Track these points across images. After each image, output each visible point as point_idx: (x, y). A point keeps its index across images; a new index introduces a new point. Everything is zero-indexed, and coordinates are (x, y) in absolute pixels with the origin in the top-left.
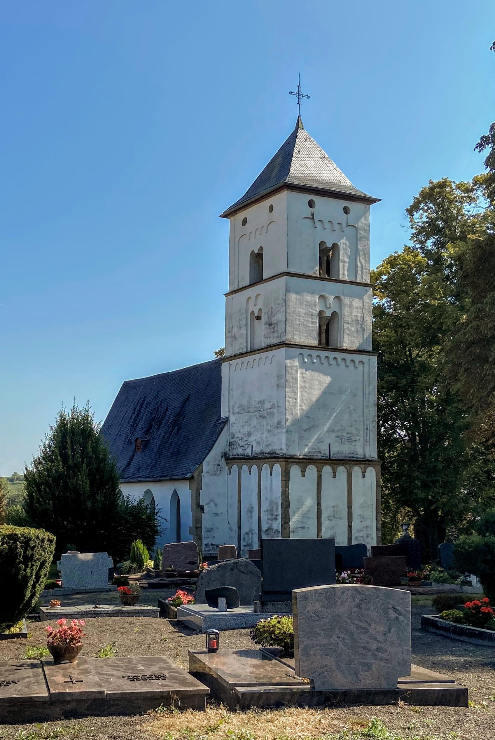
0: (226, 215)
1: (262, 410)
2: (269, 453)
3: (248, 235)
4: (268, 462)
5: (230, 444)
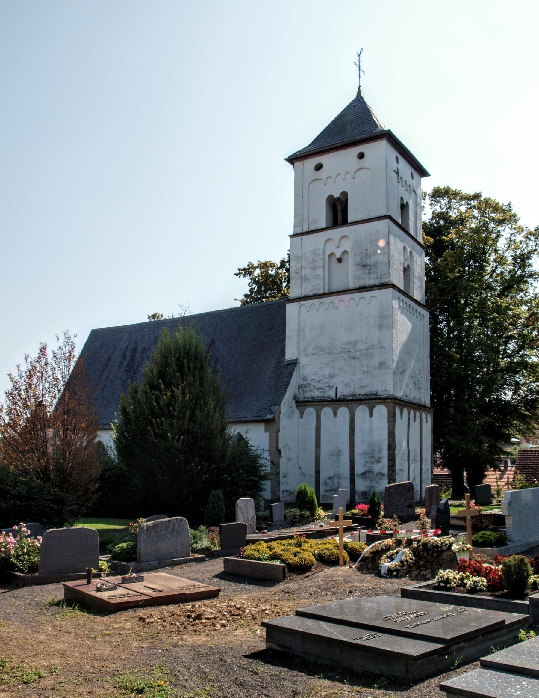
0: (292, 160)
1: (353, 351)
2: (365, 395)
3: (325, 179)
4: (366, 403)
5: (300, 387)
